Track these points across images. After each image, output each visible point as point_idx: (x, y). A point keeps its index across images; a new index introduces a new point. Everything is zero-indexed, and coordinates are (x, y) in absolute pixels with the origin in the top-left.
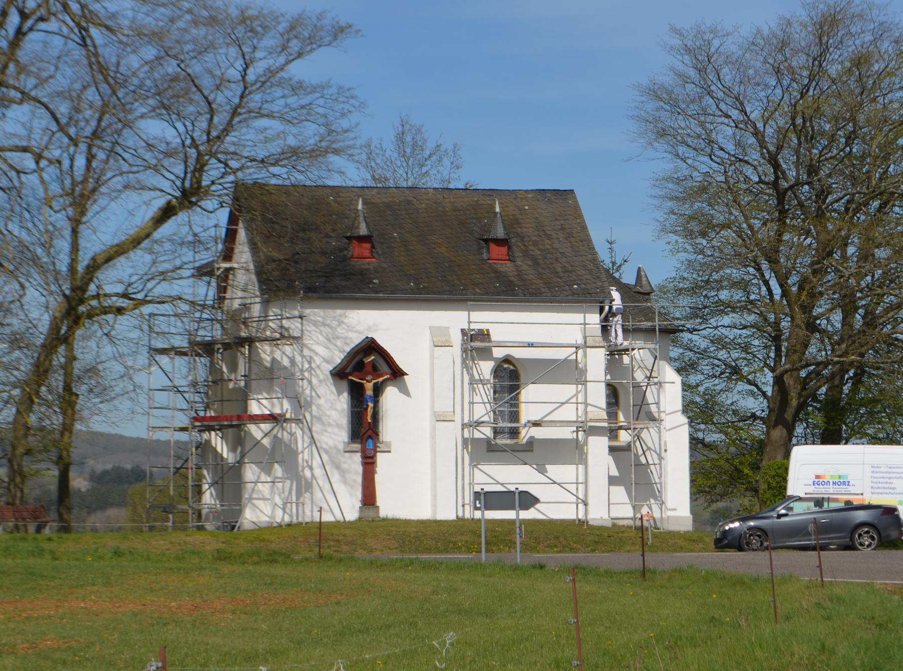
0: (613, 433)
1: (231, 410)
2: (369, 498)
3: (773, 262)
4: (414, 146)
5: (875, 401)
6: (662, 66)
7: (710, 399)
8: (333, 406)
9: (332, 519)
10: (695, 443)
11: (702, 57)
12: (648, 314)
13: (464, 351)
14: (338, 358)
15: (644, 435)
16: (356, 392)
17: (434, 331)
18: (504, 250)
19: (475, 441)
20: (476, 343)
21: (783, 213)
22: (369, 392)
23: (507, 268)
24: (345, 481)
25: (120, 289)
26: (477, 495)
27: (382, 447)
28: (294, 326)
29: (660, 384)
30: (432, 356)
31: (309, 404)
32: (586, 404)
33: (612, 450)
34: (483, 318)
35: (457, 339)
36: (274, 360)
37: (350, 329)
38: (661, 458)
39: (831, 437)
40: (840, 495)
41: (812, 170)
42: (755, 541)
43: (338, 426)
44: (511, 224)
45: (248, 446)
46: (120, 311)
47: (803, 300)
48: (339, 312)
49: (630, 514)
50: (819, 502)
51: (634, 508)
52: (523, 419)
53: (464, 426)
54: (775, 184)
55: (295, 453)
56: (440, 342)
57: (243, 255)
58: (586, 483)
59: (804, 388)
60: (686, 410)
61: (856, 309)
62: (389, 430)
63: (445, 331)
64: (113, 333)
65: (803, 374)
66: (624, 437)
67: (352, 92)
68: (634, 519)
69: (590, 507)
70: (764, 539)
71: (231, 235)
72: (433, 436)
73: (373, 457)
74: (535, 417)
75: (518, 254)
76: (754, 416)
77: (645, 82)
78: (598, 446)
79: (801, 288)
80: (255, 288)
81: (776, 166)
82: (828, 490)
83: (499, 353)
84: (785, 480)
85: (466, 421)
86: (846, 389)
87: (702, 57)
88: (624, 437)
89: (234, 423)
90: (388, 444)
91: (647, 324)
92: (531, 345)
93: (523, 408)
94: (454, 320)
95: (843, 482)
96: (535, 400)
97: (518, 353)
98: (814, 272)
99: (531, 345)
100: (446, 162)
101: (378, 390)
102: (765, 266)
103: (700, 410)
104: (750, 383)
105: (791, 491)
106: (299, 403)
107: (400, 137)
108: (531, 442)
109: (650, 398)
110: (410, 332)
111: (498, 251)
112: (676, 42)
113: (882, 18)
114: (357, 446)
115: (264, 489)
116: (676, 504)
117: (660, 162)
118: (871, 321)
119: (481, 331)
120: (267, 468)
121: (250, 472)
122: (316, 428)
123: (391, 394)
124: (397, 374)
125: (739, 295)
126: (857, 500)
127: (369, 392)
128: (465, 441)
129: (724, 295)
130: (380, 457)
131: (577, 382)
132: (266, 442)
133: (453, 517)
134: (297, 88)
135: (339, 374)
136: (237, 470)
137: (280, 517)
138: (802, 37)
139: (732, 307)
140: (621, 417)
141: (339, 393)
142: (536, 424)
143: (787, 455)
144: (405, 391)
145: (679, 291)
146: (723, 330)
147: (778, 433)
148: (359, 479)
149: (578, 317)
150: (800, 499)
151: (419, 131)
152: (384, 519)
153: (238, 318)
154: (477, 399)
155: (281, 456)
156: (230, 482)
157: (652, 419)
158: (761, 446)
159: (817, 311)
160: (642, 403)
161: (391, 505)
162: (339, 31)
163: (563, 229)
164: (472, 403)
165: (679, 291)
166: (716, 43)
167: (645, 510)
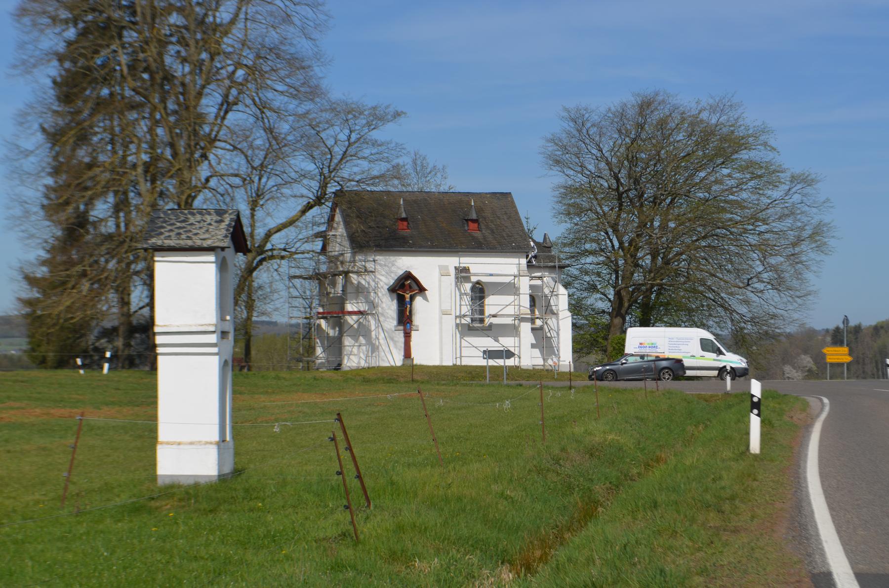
0: (533, 321)
1: (336, 308)
2: (407, 354)
3: (615, 231)
4: (422, 166)
5: (668, 304)
6: (559, 127)
7: (579, 300)
8: (389, 307)
9: (388, 365)
10: (574, 325)
11: (578, 121)
12: (552, 258)
13: (457, 278)
14: (392, 282)
15: (549, 322)
16: (401, 300)
17: (441, 268)
18: (476, 225)
19: (463, 325)
20: (462, 274)
21: (621, 205)
22: (408, 300)
23: (478, 234)
24: (396, 347)
25: (282, 246)
26: (484, 352)
27: (414, 328)
28: (370, 266)
29: (557, 295)
30: (440, 281)
31: (377, 306)
32: (520, 306)
33: (533, 329)
34: (467, 261)
35: (453, 272)
36: (359, 282)
37: (399, 268)
38: (558, 334)
39: (645, 322)
40: (653, 353)
41: (637, 182)
42: (610, 376)
43: (393, 318)
44: (479, 211)
45: (346, 328)
46: (283, 258)
47: (631, 250)
48: (392, 258)
49: (542, 363)
50: (642, 357)
51: (544, 360)
52: (487, 314)
53: (456, 317)
54: (617, 189)
55: (370, 331)
56: (444, 273)
57: (340, 230)
58: (520, 347)
59: (631, 297)
60: (570, 310)
61: (659, 255)
62: (417, 319)
63: (446, 267)
64: (280, 269)
65: (631, 289)
66: (539, 323)
67: (404, 146)
68: (544, 365)
69: (522, 360)
70: (616, 375)
71: (331, 219)
72: (441, 323)
73: (410, 333)
74: (493, 313)
75: (483, 227)
76: (604, 312)
77: (549, 136)
78: (526, 327)
79: (630, 244)
80: (347, 243)
81: (618, 180)
82: (643, 351)
83: (474, 279)
84: (624, 346)
85: (458, 314)
86: (653, 296)
87: (578, 121)
88: (539, 323)
89: (337, 315)
90: (417, 326)
91: (553, 264)
92: (491, 275)
93: (486, 308)
94: (451, 262)
95: (654, 346)
96: (493, 304)
97: (484, 279)
98: (638, 236)
99: (491, 275)
100: (439, 175)
101: (412, 298)
102: (610, 231)
103: (576, 308)
104: (602, 294)
105: (627, 351)
106: (373, 305)
107: (414, 162)
108: (491, 325)
109: (552, 303)
110: (429, 268)
111: (473, 226)
112: (565, 114)
113: (675, 102)
114: (402, 328)
115: (355, 350)
116: (565, 357)
117: (557, 178)
118: (667, 262)
119: (465, 267)
120: (355, 337)
121: (347, 341)
122: (381, 319)
123: (418, 301)
124: (422, 290)
125: (595, 246)
126: (661, 356)
127: (408, 300)
128: (457, 325)
129: (588, 246)
130: (413, 333)
131: (515, 294)
132: (355, 326)
133: (451, 364)
134: (375, 143)
135: (392, 290)
136: (339, 340)
137: (363, 364)
138: (631, 112)
139: (592, 253)
140: (537, 312)
141: (392, 300)
142: (494, 316)
143: (624, 332)
144: (426, 299)
145: (565, 245)
146: (588, 266)
147: (617, 321)
148: (403, 345)
149: (516, 261)
150: (632, 355)
151: (424, 158)
152: (422, 367)
153: (333, 260)
154: (463, 303)
155: (363, 331)
156: (335, 346)
157: (553, 313)
158: (608, 327)
159: (640, 255)
160: (548, 305)
161: (420, 357)
162: (397, 115)
163: (506, 214)
164: (461, 305)
165: (565, 245)
166: (587, 115)
167: (550, 362)
